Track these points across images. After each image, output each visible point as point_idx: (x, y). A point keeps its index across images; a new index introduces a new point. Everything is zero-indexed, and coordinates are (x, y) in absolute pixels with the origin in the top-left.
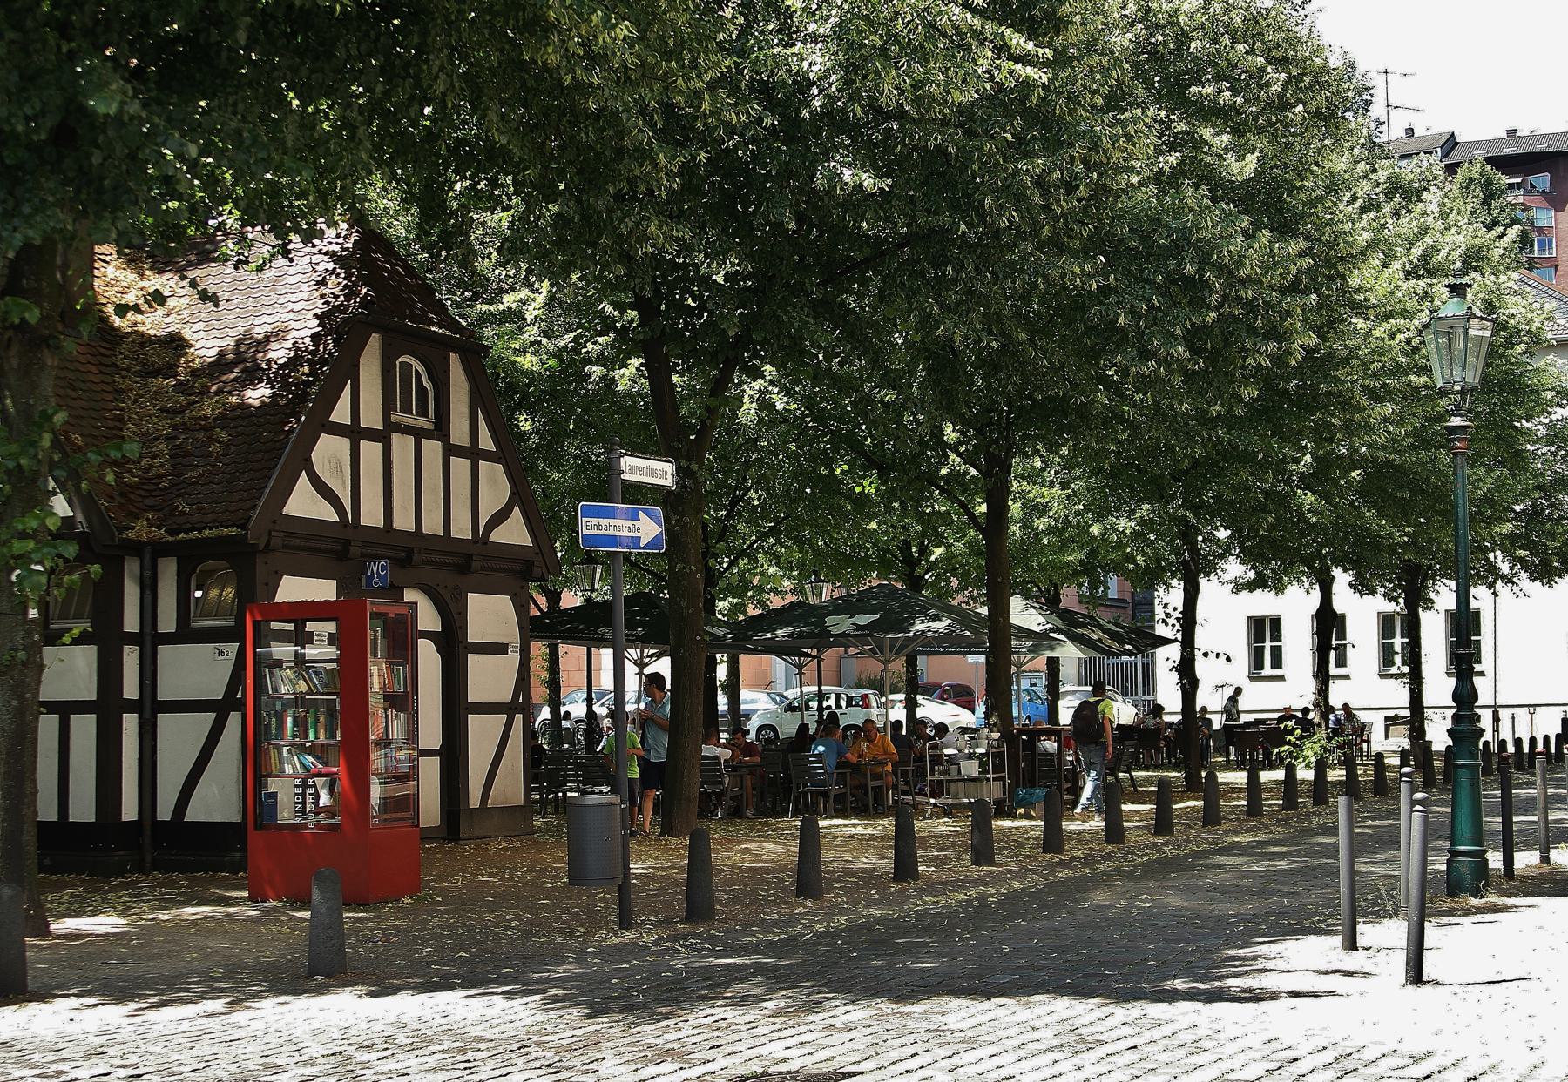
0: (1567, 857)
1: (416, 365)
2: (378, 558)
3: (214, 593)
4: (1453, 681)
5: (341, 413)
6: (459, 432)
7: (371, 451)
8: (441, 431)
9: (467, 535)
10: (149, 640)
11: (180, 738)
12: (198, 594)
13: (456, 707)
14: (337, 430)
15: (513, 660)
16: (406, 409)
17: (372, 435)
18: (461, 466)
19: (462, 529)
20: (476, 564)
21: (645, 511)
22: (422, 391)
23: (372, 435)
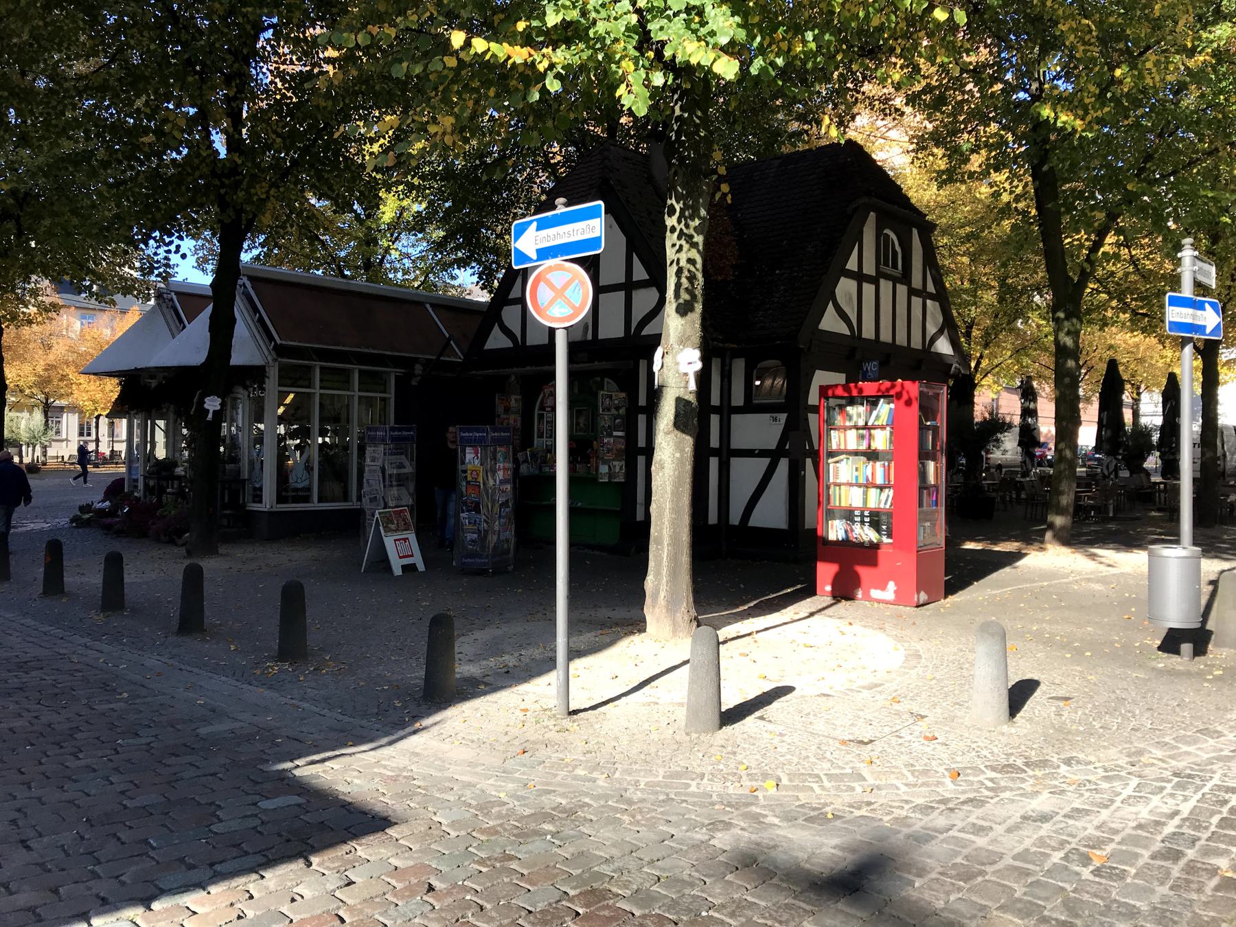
1: (893, 236)
3: (768, 382)
5: (852, 265)
6: (917, 282)
7: (868, 289)
8: (906, 278)
9: (920, 347)
10: (727, 411)
11: (746, 474)
12: (758, 383)
14: (849, 274)
16: (886, 264)
18: (917, 301)
21: (1211, 304)
22: (895, 253)
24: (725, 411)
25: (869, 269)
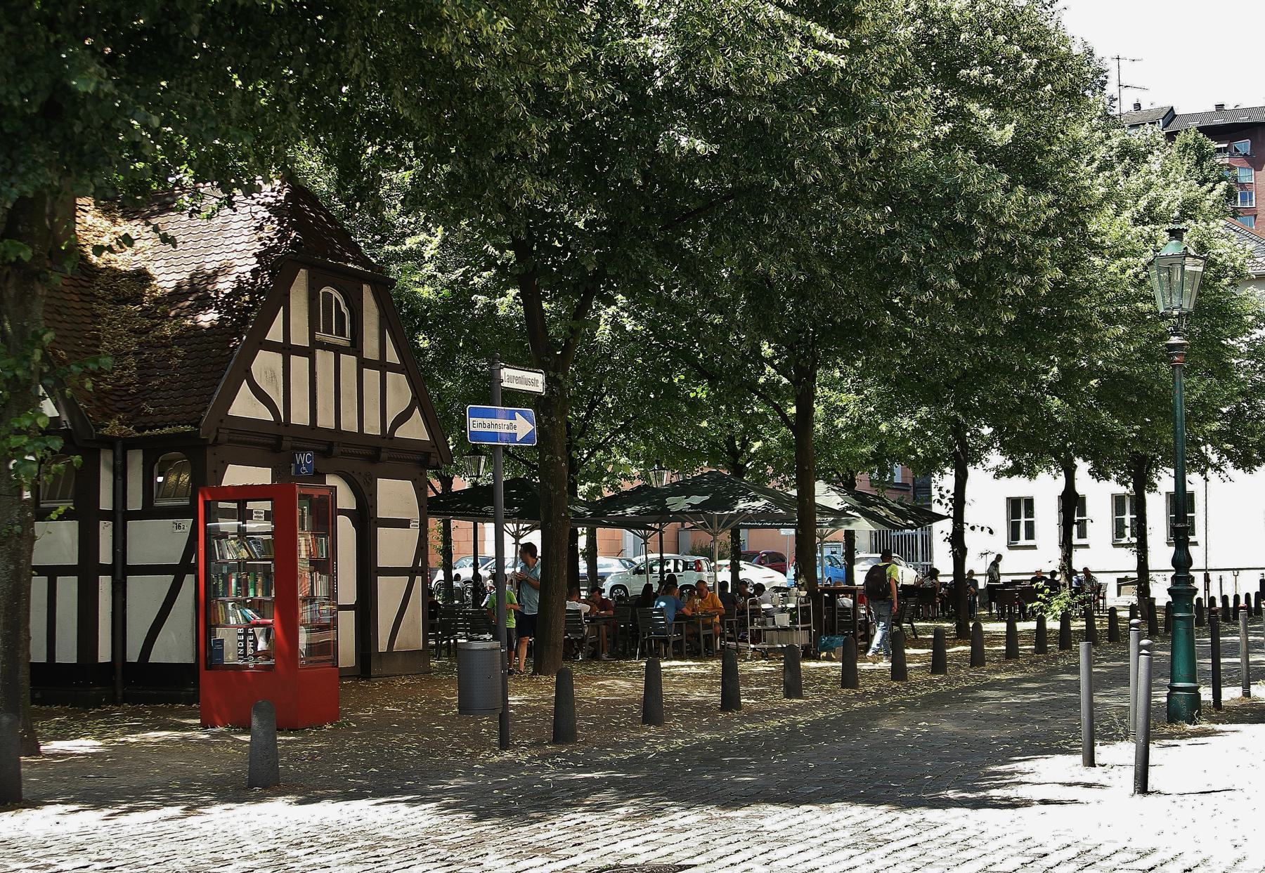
0: (1264, 692)
1: (336, 295)
2: (305, 450)
3: (173, 479)
4: (1173, 549)
5: (275, 333)
6: (370, 348)
7: (299, 364)
8: (355, 347)
9: (377, 431)
10: (120, 517)
11: (145, 595)
12: (160, 479)
13: (368, 571)
14: (272, 346)
15: (414, 532)
16: (328, 330)
17: (300, 351)
18: (372, 376)
19: (372, 427)
20: (384, 455)
22: (340, 315)
23: (300, 351)
24: (119, 516)
25: (300, 337)
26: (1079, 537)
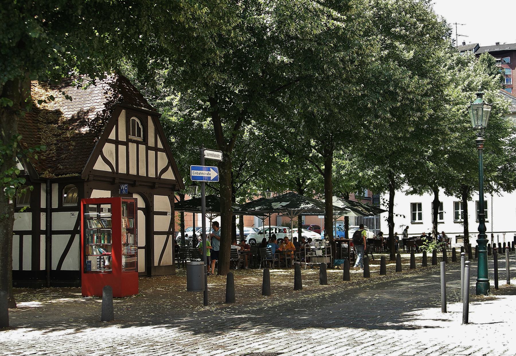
1: (137, 120)
2: (125, 184)
3: (70, 195)
4: (478, 224)
5: (112, 136)
6: (151, 142)
7: (122, 148)
8: (145, 142)
9: (154, 176)
10: (49, 211)
11: (59, 243)
12: (65, 195)
13: (150, 233)
14: (111, 141)
15: (169, 217)
16: (134, 135)
17: (122, 143)
18: (152, 153)
19: (152, 174)
20: (156, 186)
21: (212, 168)
22: (139, 129)
23: (122, 143)
26: (440, 219)
